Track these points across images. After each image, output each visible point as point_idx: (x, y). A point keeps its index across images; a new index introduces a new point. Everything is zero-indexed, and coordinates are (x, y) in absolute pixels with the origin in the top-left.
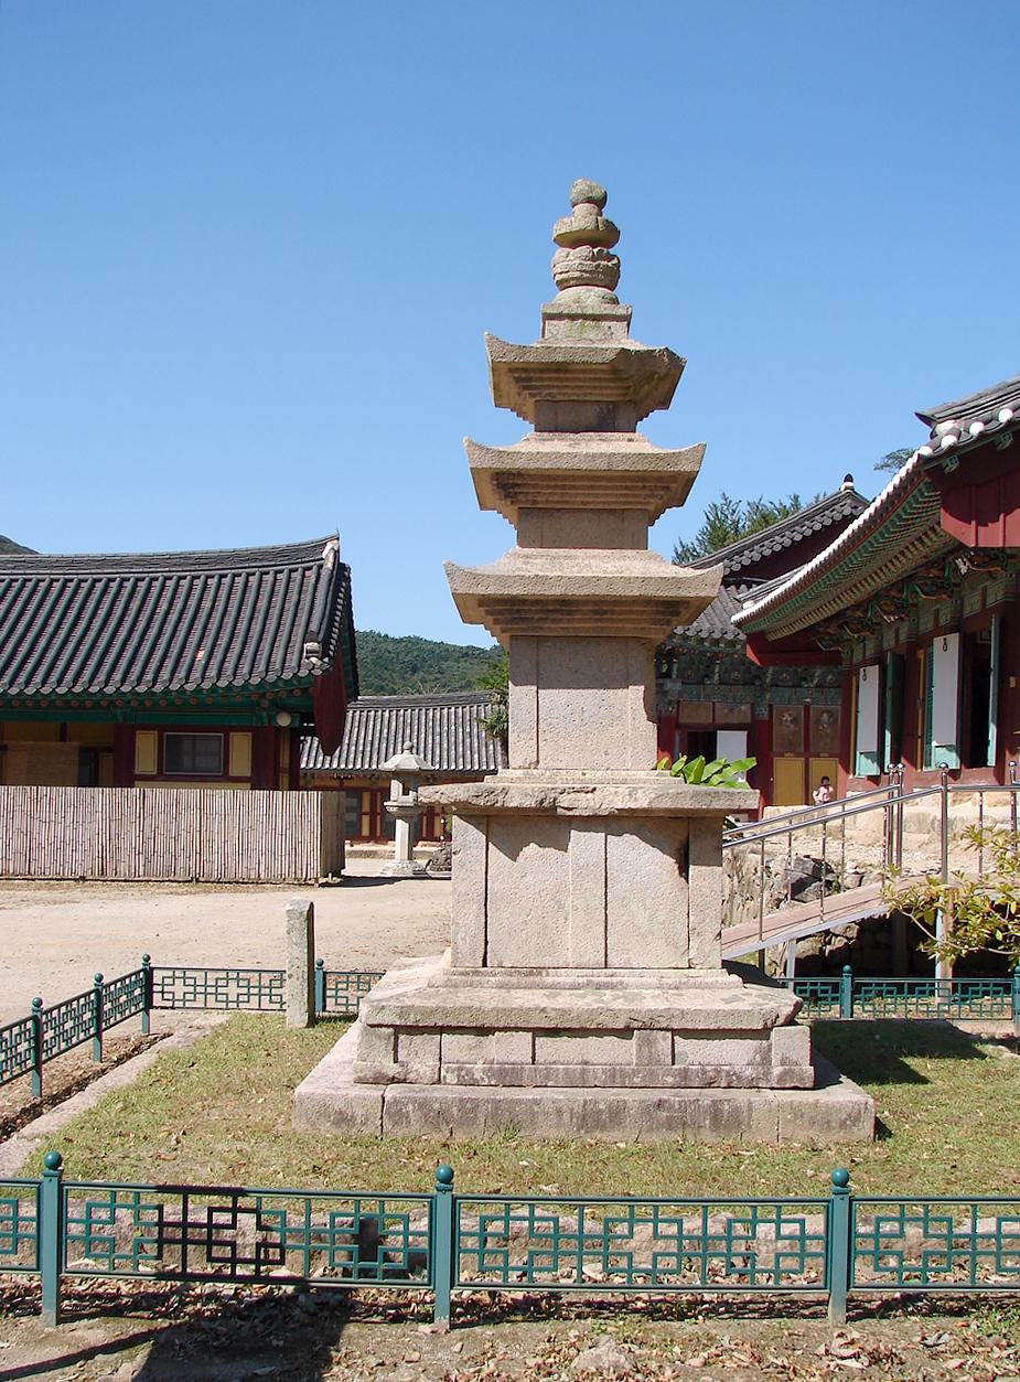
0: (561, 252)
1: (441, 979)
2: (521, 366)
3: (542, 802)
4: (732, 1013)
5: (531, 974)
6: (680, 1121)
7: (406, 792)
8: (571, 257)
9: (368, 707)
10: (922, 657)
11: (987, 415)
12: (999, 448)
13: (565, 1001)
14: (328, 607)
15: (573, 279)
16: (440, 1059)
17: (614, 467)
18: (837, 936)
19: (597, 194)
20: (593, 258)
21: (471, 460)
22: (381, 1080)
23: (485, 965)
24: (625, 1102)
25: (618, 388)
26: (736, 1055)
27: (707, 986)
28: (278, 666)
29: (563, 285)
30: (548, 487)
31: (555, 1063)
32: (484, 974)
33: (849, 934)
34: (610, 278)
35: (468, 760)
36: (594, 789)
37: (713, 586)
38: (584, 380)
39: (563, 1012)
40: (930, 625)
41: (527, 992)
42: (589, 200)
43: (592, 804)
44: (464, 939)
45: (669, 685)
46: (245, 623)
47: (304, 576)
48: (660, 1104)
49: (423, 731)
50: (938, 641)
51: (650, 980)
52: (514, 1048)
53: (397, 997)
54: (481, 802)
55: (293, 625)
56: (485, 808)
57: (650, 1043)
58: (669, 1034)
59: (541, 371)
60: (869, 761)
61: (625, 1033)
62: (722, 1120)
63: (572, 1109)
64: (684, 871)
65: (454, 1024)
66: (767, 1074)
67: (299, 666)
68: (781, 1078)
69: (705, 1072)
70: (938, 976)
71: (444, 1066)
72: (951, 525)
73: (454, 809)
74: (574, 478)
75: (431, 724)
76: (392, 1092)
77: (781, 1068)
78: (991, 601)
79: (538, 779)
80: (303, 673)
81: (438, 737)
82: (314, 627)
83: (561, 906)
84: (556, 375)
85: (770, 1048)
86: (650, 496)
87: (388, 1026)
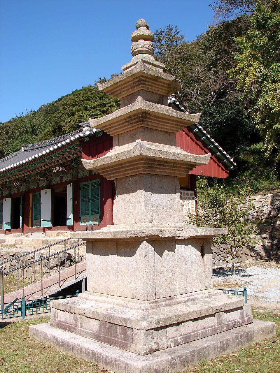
15: (145, 51)
20: (152, 46)
21: (140, 105)
24: (229, 339)
30: (155, 120)
44: (150, 289)
50: (43, 191)
52: (188, 328)
59: (150, 79)
61: (213, 315)
63: (218, 346)
64: (203, 256)
66: (244, 320)
73: (147, 238)
77: (247, 318)
83: (175, 273)
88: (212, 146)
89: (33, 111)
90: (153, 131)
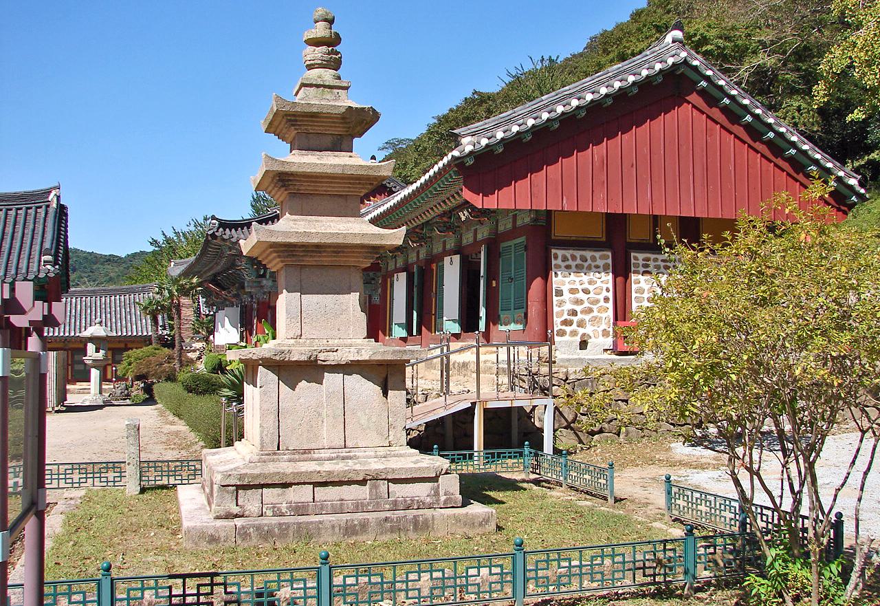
0: (310, 49)
1: (256, 458)
2: (293, 113)
3: (310, 358)
4: (419, 469)
5: (305, 453)
6: (397, 528)
7: (97, 351)
8: (316, 52)
9: (82, 294)
10: (434, 268)
11: (489, 134)
12: (495, 153)
13: (328, 467)
14: (56, 232)
15: (318, 64)
16: (262, 503)
17: (346, 172)
18: (413, 430)
19: (329, 17)
21: (266, 166)
22: (229, 516)
23: (279, 449)
24: (368, 519)
25: (344, 127)
26: (421, 491)
27: (401, 456)
28: (24, 271)
29: (310, 67)
30: (307, 182)
31: (325, 501)
32: (279, 454)
33: (420, 429)
34: (335, 64)
35: (129, 329)
36: (337, 350)
37: (400, 239)
38: (326, 122)
39: (330, 473)
40: (440, 249)
41: (305, 463)
42: (326, 20)
43: (336, 358)
44: (266, 435)
45: (264, 282)
46: (27, 249)
47: (36, 212)
48: (386, 519)
49: (99, 311)
50: (447, 260)
51: (370, 453)
52: (302, 494)
53: (235, 469)
54: (277, 358)
55: (32, 244)
56: (279, 361)
57: (376, 487)
58: (386, 482)
59: (303, 116)
60: (401, 329)
61: (363, 482)
62: (420, 526)
63: (340, 525)
64: (385, 394)
65: (270, 482)
66: (438, 500)
67: (39, 271)
68: (445, 502)
69: (405, 501)
70: (476, 449)
71: (265, 507)
72: (467, 195)
73: (261, 362)
74: (322, 177)
75: (104, 306)
76: (239, 522)
77: (445, 497)
78: (479, 237)
79: (304, 345)
80: (42, 275)
81: (109, 315)
82: (47, 245)
84: (311, 119)
85: (438, 486)
86: (363, 188)
87: (233, 486)
88: (793, 151)
89: (546, 58)
90: (311, 197)
